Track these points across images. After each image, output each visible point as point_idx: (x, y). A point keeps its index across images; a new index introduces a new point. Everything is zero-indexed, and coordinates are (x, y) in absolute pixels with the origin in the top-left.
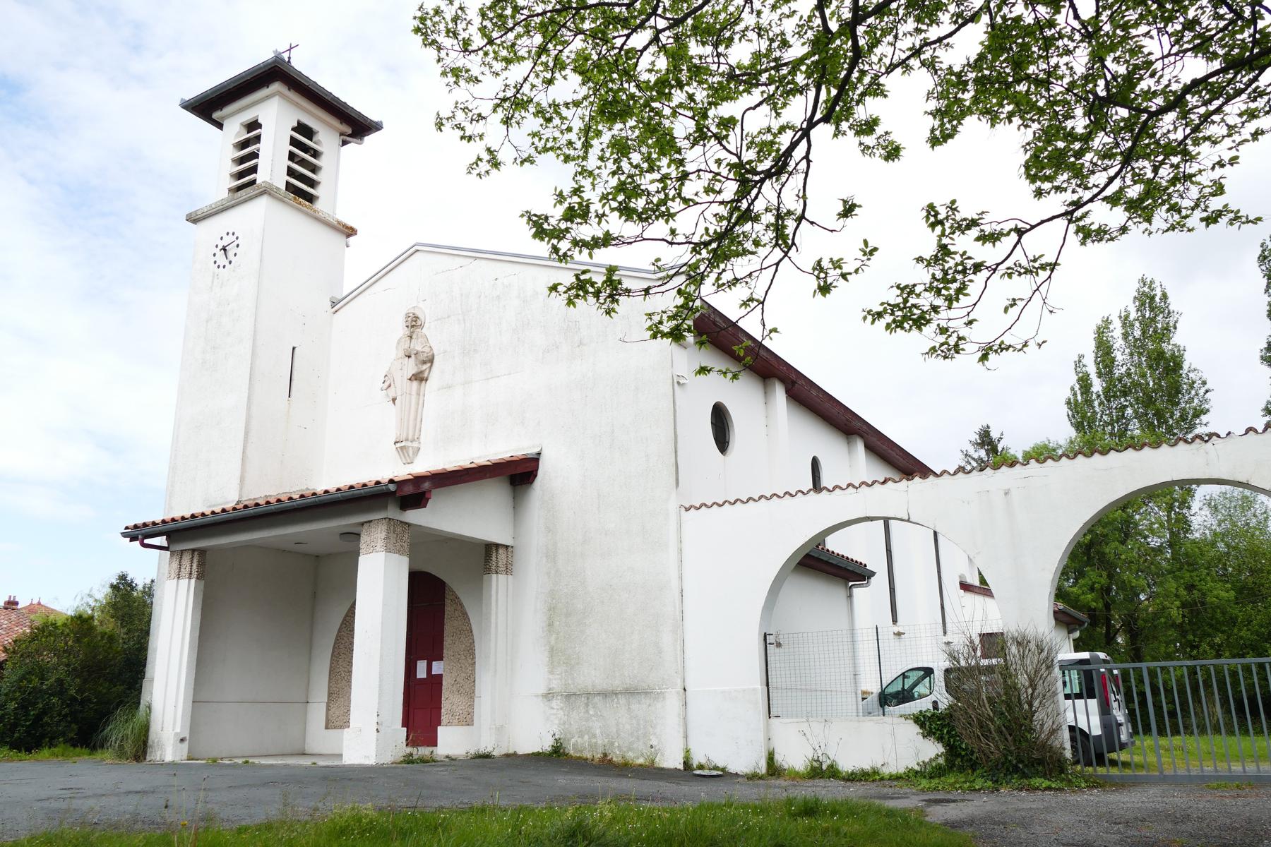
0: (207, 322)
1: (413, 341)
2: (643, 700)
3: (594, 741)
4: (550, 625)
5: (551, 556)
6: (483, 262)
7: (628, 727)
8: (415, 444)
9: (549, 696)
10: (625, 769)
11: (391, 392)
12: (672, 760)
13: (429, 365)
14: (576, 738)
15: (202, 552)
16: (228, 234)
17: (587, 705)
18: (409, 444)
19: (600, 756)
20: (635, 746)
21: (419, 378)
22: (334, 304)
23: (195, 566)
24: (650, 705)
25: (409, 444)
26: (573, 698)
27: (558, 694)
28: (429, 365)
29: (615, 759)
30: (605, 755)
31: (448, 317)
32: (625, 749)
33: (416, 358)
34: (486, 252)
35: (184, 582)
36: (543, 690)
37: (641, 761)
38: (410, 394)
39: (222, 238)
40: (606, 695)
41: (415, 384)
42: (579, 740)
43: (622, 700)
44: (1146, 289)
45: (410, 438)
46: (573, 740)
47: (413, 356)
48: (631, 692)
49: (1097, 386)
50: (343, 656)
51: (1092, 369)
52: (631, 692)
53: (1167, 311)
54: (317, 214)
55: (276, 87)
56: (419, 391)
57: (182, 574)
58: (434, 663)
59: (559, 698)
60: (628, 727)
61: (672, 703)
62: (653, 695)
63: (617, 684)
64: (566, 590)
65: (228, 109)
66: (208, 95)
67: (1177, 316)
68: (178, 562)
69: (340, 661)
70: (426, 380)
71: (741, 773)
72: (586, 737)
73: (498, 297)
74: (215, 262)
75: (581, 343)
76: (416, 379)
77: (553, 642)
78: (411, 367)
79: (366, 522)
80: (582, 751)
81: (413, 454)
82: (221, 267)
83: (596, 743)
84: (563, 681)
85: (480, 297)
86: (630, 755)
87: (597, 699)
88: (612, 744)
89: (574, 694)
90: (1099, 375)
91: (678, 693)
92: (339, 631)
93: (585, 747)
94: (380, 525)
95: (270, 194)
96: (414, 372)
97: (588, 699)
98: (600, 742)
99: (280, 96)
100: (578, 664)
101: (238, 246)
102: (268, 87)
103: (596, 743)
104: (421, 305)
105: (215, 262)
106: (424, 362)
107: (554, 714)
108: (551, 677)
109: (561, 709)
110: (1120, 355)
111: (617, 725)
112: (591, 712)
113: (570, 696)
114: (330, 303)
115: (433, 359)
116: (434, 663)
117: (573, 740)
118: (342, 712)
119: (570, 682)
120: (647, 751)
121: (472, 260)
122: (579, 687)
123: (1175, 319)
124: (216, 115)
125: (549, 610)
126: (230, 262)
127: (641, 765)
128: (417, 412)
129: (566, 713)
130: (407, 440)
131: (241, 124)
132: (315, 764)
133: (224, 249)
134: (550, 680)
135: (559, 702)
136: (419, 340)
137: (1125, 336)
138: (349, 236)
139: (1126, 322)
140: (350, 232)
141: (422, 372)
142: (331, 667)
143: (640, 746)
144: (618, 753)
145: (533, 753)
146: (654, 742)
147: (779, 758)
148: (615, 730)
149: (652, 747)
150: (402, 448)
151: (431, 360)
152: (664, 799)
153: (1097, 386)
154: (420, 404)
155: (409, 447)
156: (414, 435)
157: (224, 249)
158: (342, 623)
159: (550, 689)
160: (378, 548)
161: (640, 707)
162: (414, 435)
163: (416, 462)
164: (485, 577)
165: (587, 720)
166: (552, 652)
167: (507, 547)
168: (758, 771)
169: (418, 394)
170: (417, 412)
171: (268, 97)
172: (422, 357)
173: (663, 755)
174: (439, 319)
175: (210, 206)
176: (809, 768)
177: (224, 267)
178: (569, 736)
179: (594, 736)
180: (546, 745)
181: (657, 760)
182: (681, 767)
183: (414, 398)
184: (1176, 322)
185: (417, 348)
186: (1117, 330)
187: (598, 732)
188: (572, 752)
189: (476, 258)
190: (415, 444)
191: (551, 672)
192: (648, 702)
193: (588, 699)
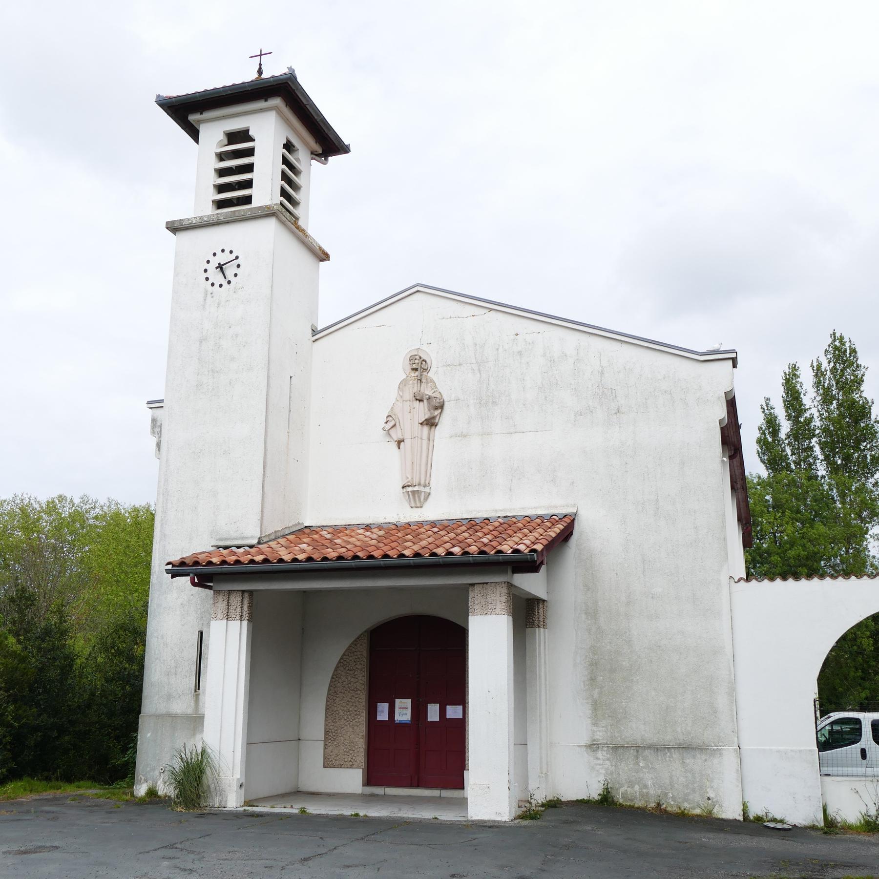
0: (201, 341)
1: (423, 384)
2: (699, 756)
3: (645, 791)
4: (592, 679)
5: (592, 613)
6: (500, 315)
7: (682, 779)
8: (427, 490)
9: (593, 746)
10: (682, 819)
11: (396, 435)
12: (731, 811)
13: (440, 411)
14: (625, 788)
15: (251, 593)
16: (223, 251)
17: (637, 757)
18: (422, 489)
19: (653, 805)
20: (691, 797)
21: (431, 423)
22: (314, 332)
23: (246, 608)
24: (706, 760)
25: (422, 489)
26: (620, 751)
27: (604, 745)
28: (440, 411)
29: (669, 809)
30: (659, 805)
31: (460, 365)
32: (680, 800)
33: (429, 403)
34: (561, 318)
35: (235, 625)
36: (585, 740)
37: (698, 811)
38: (422, 439)
39: (215, 254)
40: (659, 749)
41: (426, 429)
42: (629, 790)
43: (676, 755)
44: (837, 343)
45: (422, 482)
46: (622, 790)
47: (425, 401)
48: (686, 748)
49: (785, 427)
50: (340, 695)
51: (780, 413)
52: (686, 748)
53: (855, 365)
54: (306, 240)
55: (277, 102)
56: (429, 434)
57: (231, 615)
58: (448, 707)
59: (605, 749)
60: (682, 779)
61: (729, 759)
62: (709, 751)
63: (668, 738)
64: (608, 647)
65: (208, 115)
66: (196, 97)
67: (864, 370)
68: (225, 603)
69: (338, 699)
70: (436, 426)
71: (799, 826)
72: (637, 787)
73: (520, 353)
74: (207, 279)
75: (618, 411)
76: (427, 424)
77: (596, 696)
78: (422, 412)
79: (477, 584)
80: (632, 800)
81: (424, 499)
82: (210, 282)
83: (647, 793)
84: (609, 734)
85: (497, 349)
86: (686, 805)
87: (647, 752)
88: (666, 794)
89: (622, 746)
90: (789, 417)
91: (735, 750)
92: (336, 670)
93: (635, 797)
94: (498, 587)
95: (277, 217)
96: (427, 417)
97: (638, 752)
98: (652, 792)
99: (277, 112)
100: (625, 718)
101: (238, 266)
102: (266, 100)
103: (647, 793)
104: (425, 347)
105: (207, 279)
106: (436, 408)
107: (600, 765)
108: (595, 728)
109: (608, 759)
110: (810, 398)
111: (671, 777)
112: (641, 764)
113: (616, 748)
114: (311, 331)
115: (443, 405)
116: (448, 707)
117: (622, 790)
118: (342, 751)
119: (617, 735)
120: (704, 803)
121: (486, 311)
122: (627, 740)
123: (862, 373)
124: (192, 118)
125: (591, 665)
126: (229, 282)
127: (698, 816)
128: (428, 457)
129: (614, 764)
130: (419, 485)
131: (224, 132)
132: (436, 818)
133: (220, 267)
134: (594, 732)
135: (604, 753)
136: (429, 384)
137: (818, 384)
138: (322, 260)
139: (819, 372)
140: (323, 256)
141: (434, 418)
142: (327, 705)
143: (697, 797)
144: (672, 803)
145: (578, 800)
146: (711, 794)
147: (831, 811)
148: (668, 782)
149: (709, 799)
150: (413, 492)
151: (441, 407)
152: (863, 866)
153: (785, 427)
154: (430, 450)
155: (421, 492)
156: (426, 480)
157: (220, 267)
158: (339, 662)
159: (594, 740)
160: (497, 611)
161: (695, 762)
162: (426, 480)
163: (426, 505)
164: (529, 630)
165: (637, 771)
166: (596, 705)
167: (545, 600)
168: (817, 824)
169: (429, 439)
170: (428, 457)
171: (262, 110)
172: (435, 403)
173: (721, 806)
174: (447, 366)
175: (201, 218)
176: (862, 822)
177: (221, 286)
178: (617, 786)
179: (646, 786)
180: (594, 792)
181: (715, 811)
182: (741, 818)
183: (425, 442)
184: (863, 375)
185: (427, 393)
186: (806, 381)
187: (649, 783)
188: (621, 801)
189: (491, 310)
190: (427, 490)
191: (595, 724)
192: (704, 757)
193: (638, 752)
